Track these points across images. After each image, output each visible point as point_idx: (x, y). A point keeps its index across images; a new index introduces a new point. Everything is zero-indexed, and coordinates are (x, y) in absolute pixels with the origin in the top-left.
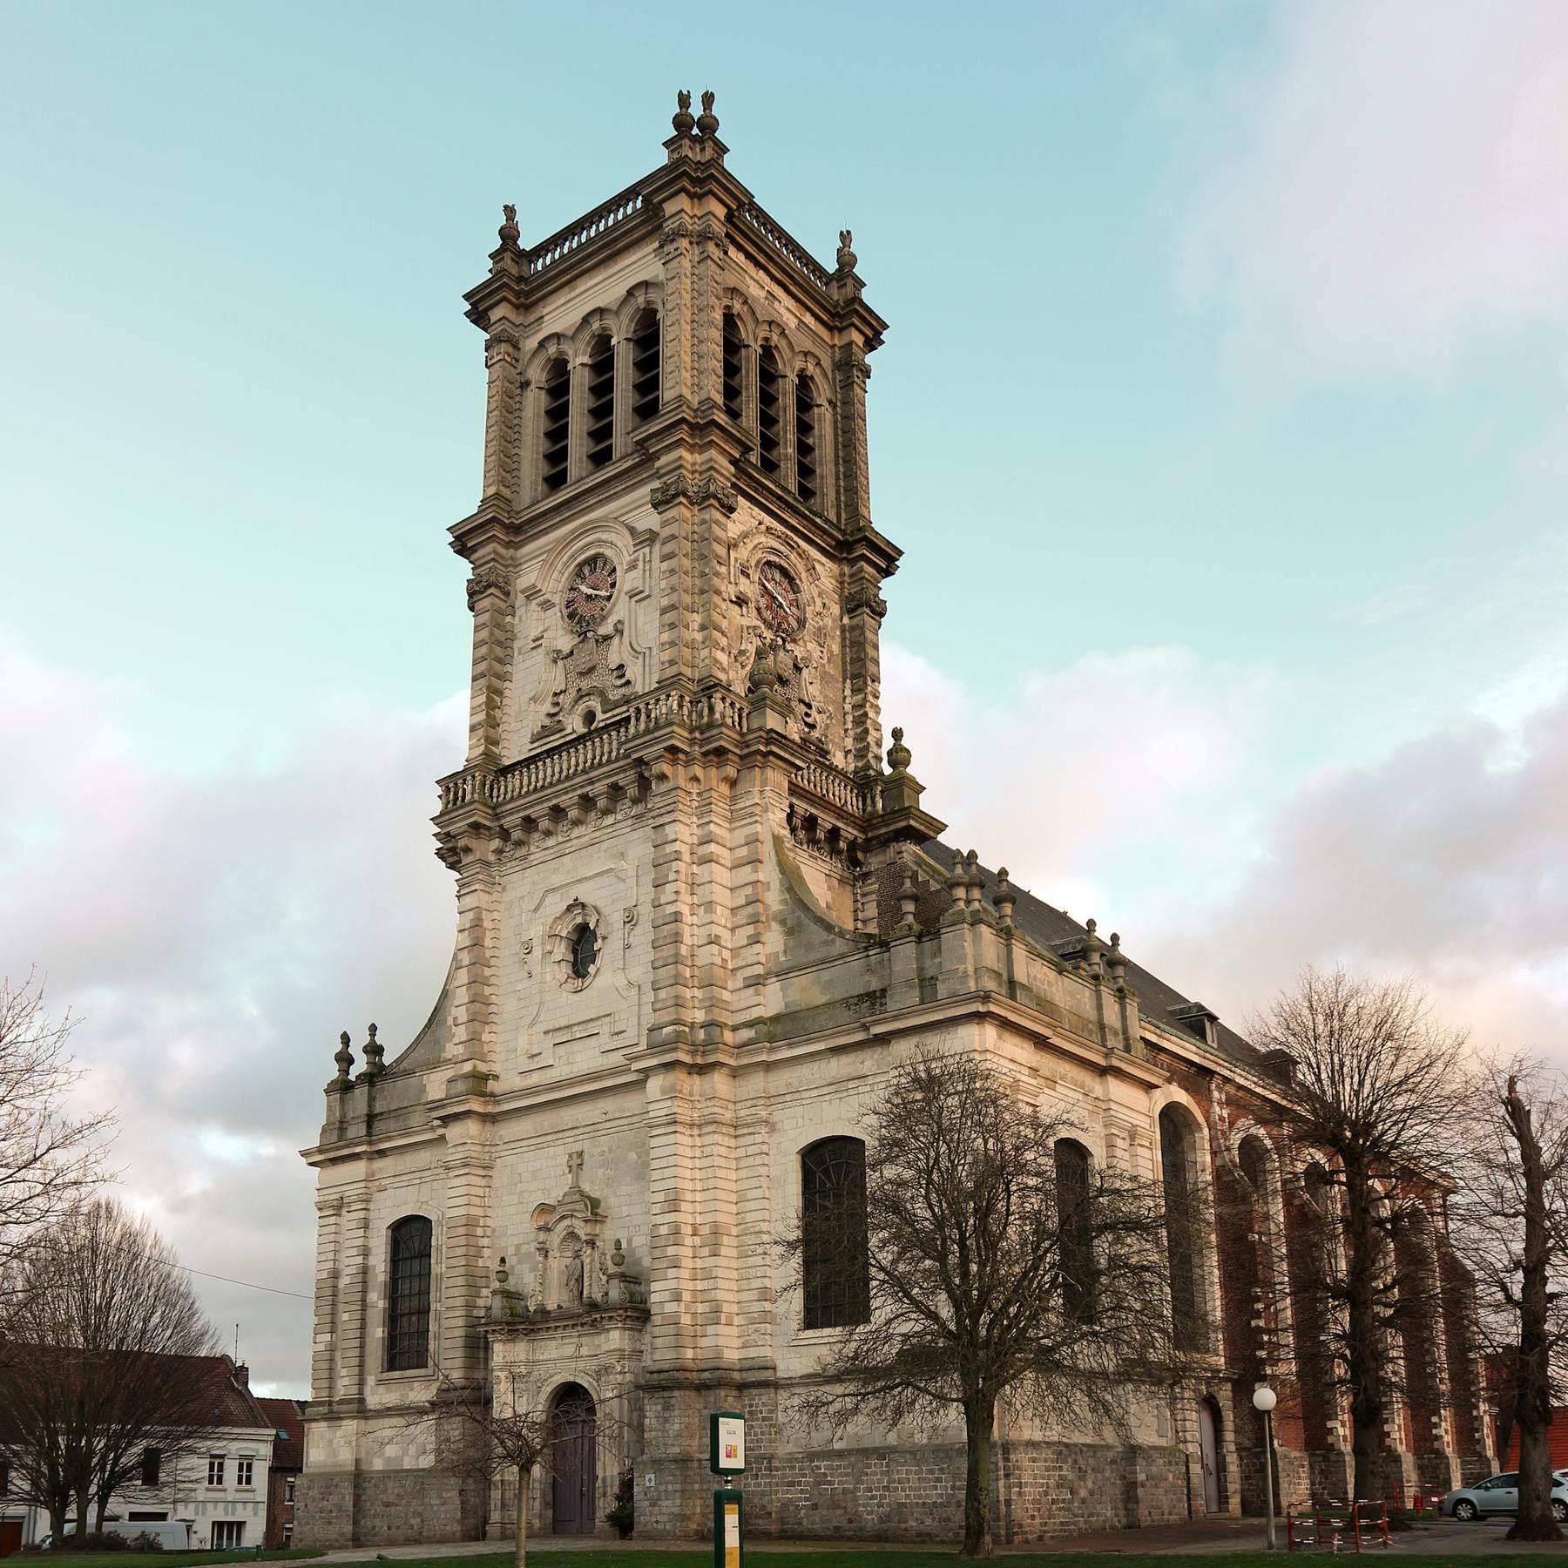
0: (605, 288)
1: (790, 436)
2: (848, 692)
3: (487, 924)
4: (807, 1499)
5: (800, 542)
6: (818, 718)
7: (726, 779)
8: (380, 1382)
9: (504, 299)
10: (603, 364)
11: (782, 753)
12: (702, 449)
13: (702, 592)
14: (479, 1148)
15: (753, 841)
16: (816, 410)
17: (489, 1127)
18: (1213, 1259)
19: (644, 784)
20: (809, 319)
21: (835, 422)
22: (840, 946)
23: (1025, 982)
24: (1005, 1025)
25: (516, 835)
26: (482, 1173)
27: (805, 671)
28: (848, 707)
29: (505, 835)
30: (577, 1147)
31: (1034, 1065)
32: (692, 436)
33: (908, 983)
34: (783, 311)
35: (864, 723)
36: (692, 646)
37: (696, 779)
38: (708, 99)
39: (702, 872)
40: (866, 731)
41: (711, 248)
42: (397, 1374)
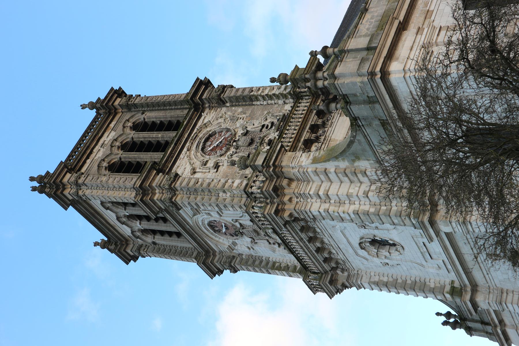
1: (154, 135)
2: (258, 103)
3: (376, 279)
5: (197, 127)
6: (269, 120)
7: (289, 185)
9: (125, 250)
11: (274, 158)
12: (153, 189)
13: (209, 191)
14: (491, 295)
15: (316, 172)
16: (146, 120)
17: (479, 289)
20: (112, 125)
21: (150, 110)
22: (360, 137)
23: (368, 39)
24: (390, 56)
25: (333, 265)
26: (505, 294)
27: (249, 129)
28: (265, 103)
29: (334, 269)
31: (415, 31)
32: (148, 194)
33: (373, 109)
34: (108, 139)
35: (270, 96)
36: (233, 197)
37: (290, 200)
38: (32, 179)
39: (333, 199)
40: (274, 94)
41: (80, 181)
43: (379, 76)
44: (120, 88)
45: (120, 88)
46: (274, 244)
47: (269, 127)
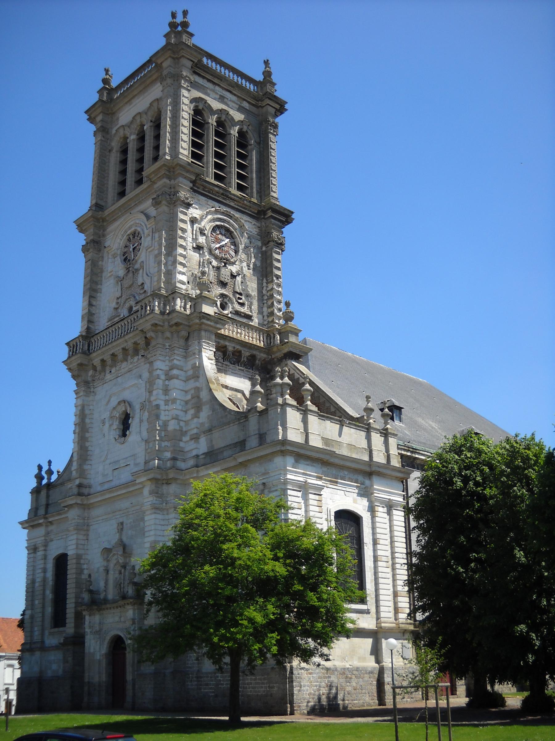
0: (141, 104)
3: (87, 412)
4: (213, 692)
8: (51, 634)
10: (142, 138)
18: (153, 717)
19: (148, 342)
30: (121, 520)
38: (185, 13)
42: (56, 630)
43: (283, 448)
44: (286, 110)
45: (286, 110)
46: (117, 303)
47: (239, 301)
